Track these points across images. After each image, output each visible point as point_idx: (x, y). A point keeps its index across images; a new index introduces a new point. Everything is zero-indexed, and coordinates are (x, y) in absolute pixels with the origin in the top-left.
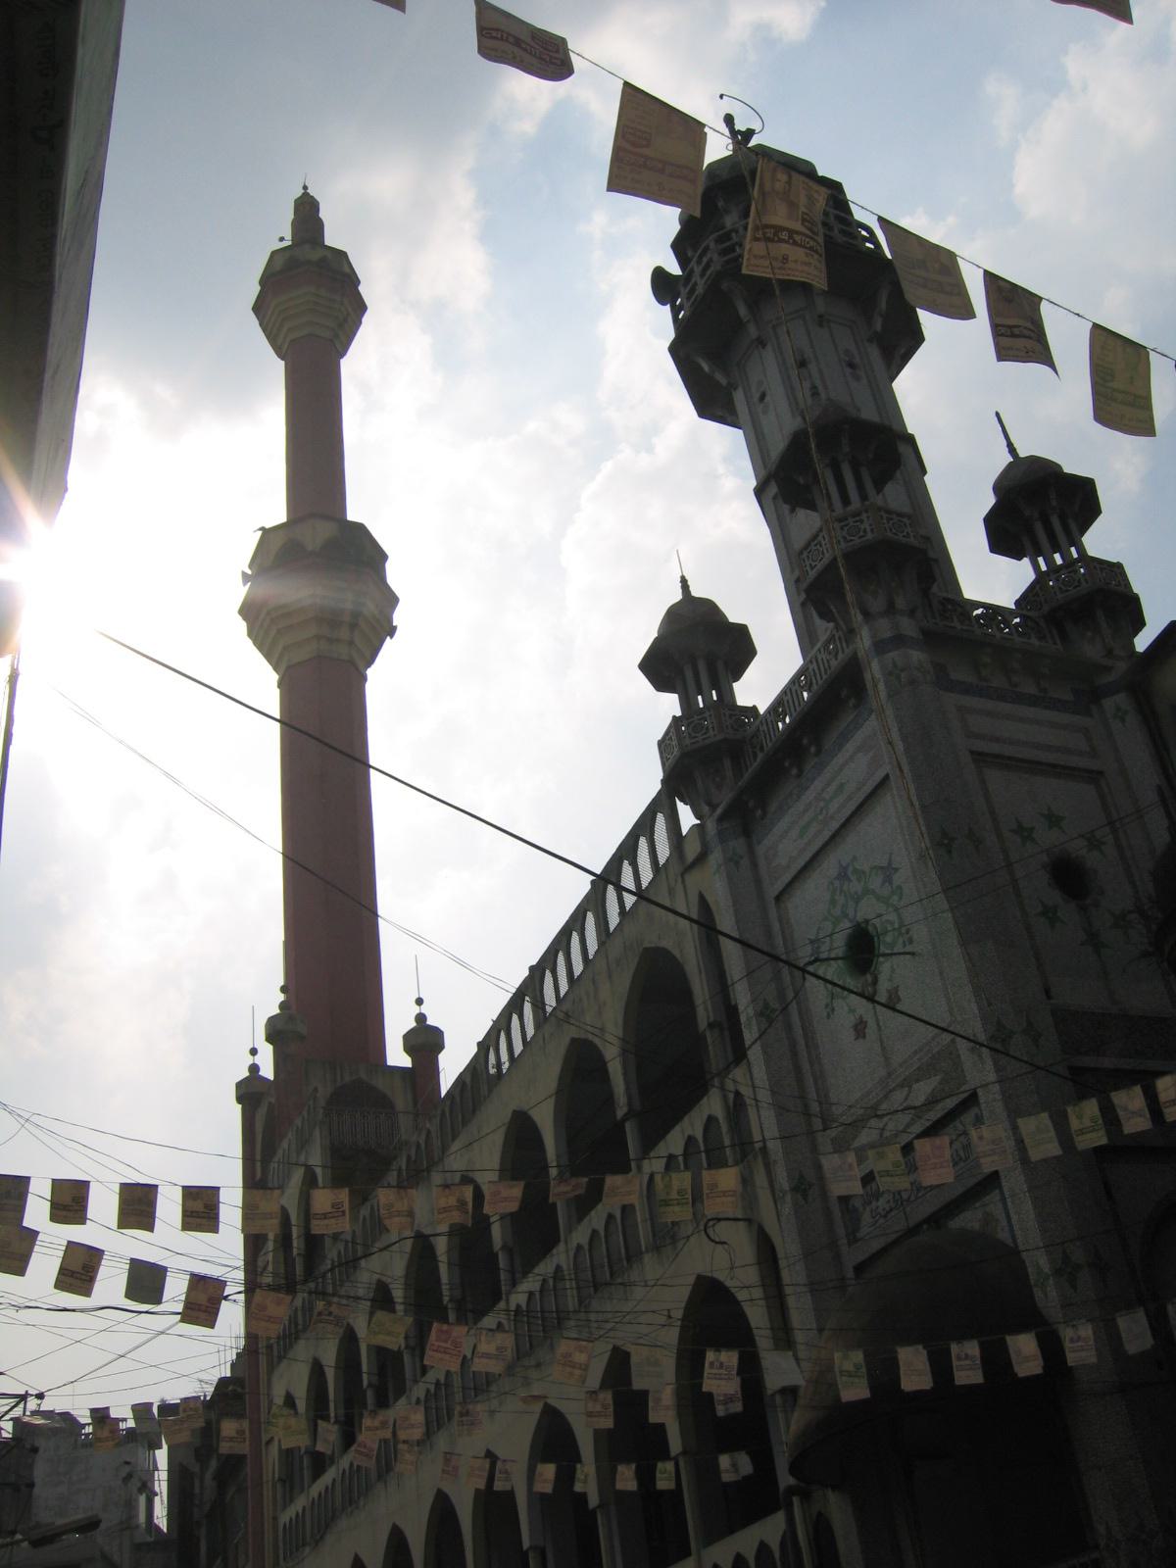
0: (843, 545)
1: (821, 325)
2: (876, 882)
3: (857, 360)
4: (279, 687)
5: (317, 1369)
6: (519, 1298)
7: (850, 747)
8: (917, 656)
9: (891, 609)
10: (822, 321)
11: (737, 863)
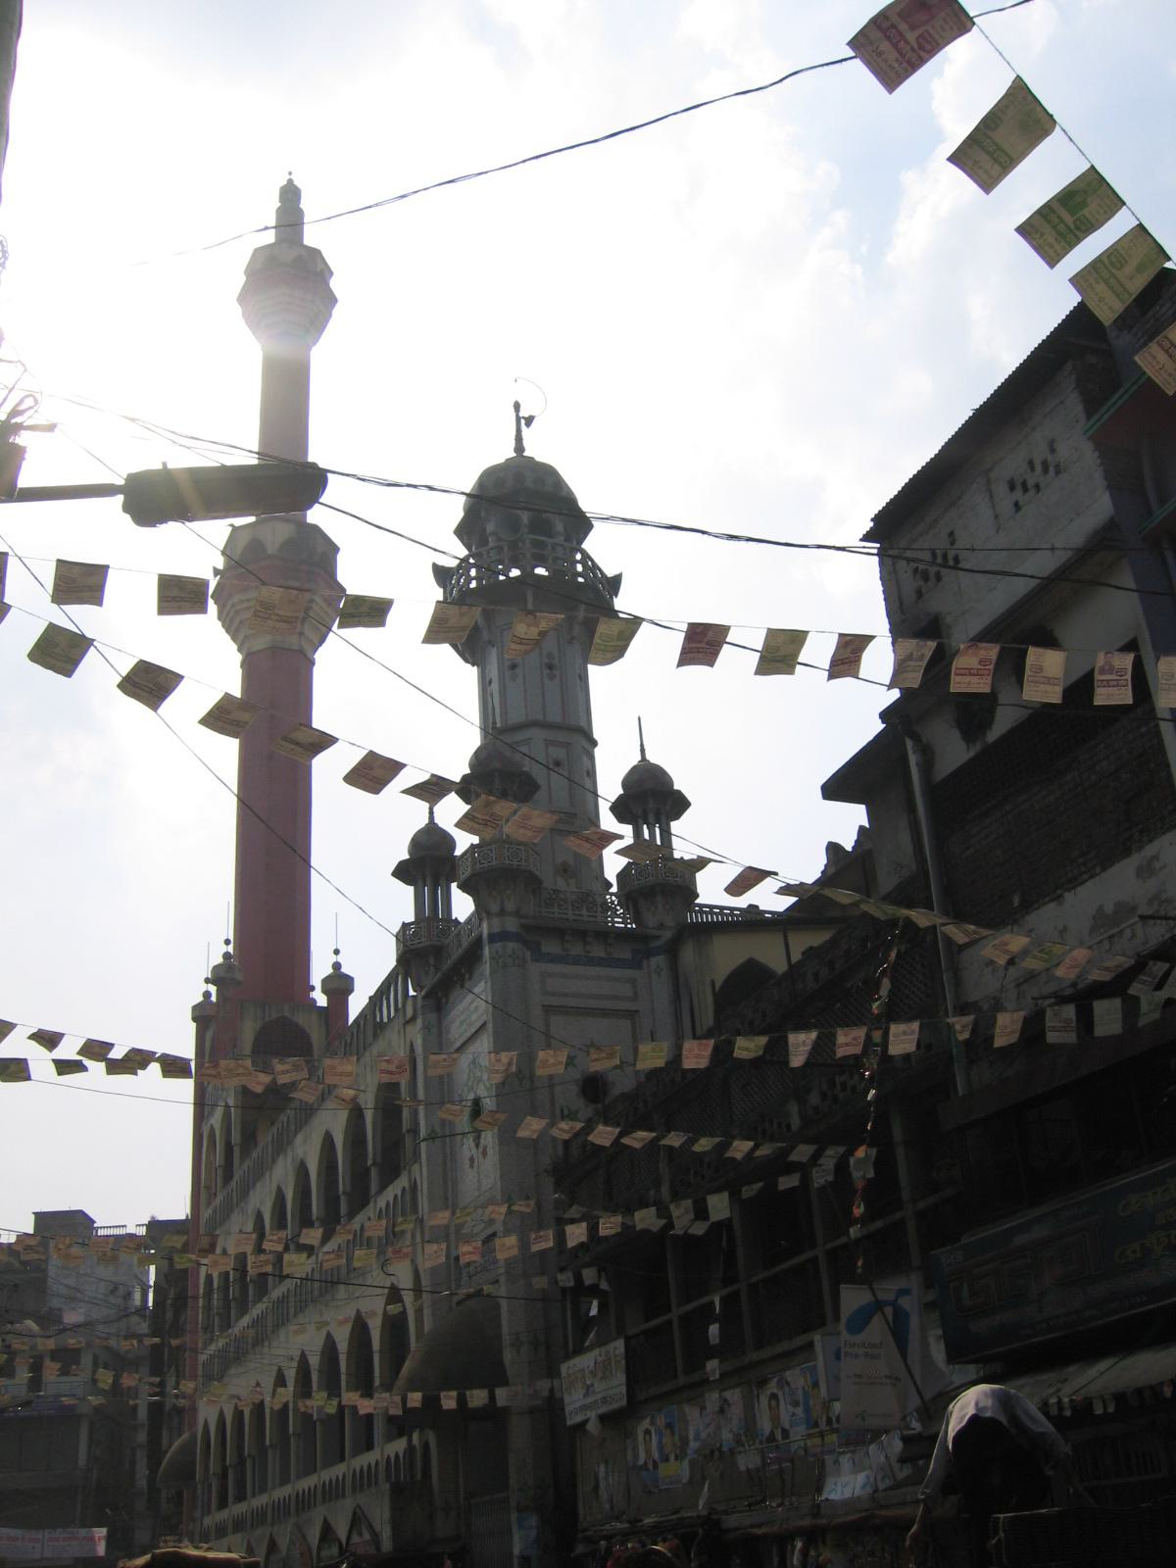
5: (302, 1171)
6: (381, 1203)
11: (430, 1030)
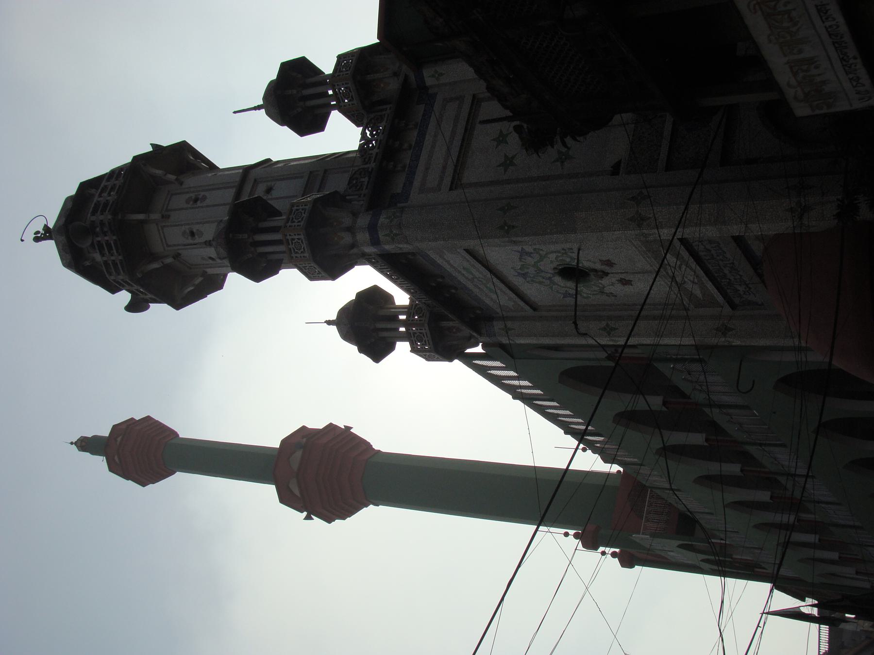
0: (306, 255)
1: (169, 217)
2: (530, 260)
3: (193, 195)
4: (378, 505)
7: (440, 261)
8: (383, 220)
9: (350, 229)
10: (166, 217)
